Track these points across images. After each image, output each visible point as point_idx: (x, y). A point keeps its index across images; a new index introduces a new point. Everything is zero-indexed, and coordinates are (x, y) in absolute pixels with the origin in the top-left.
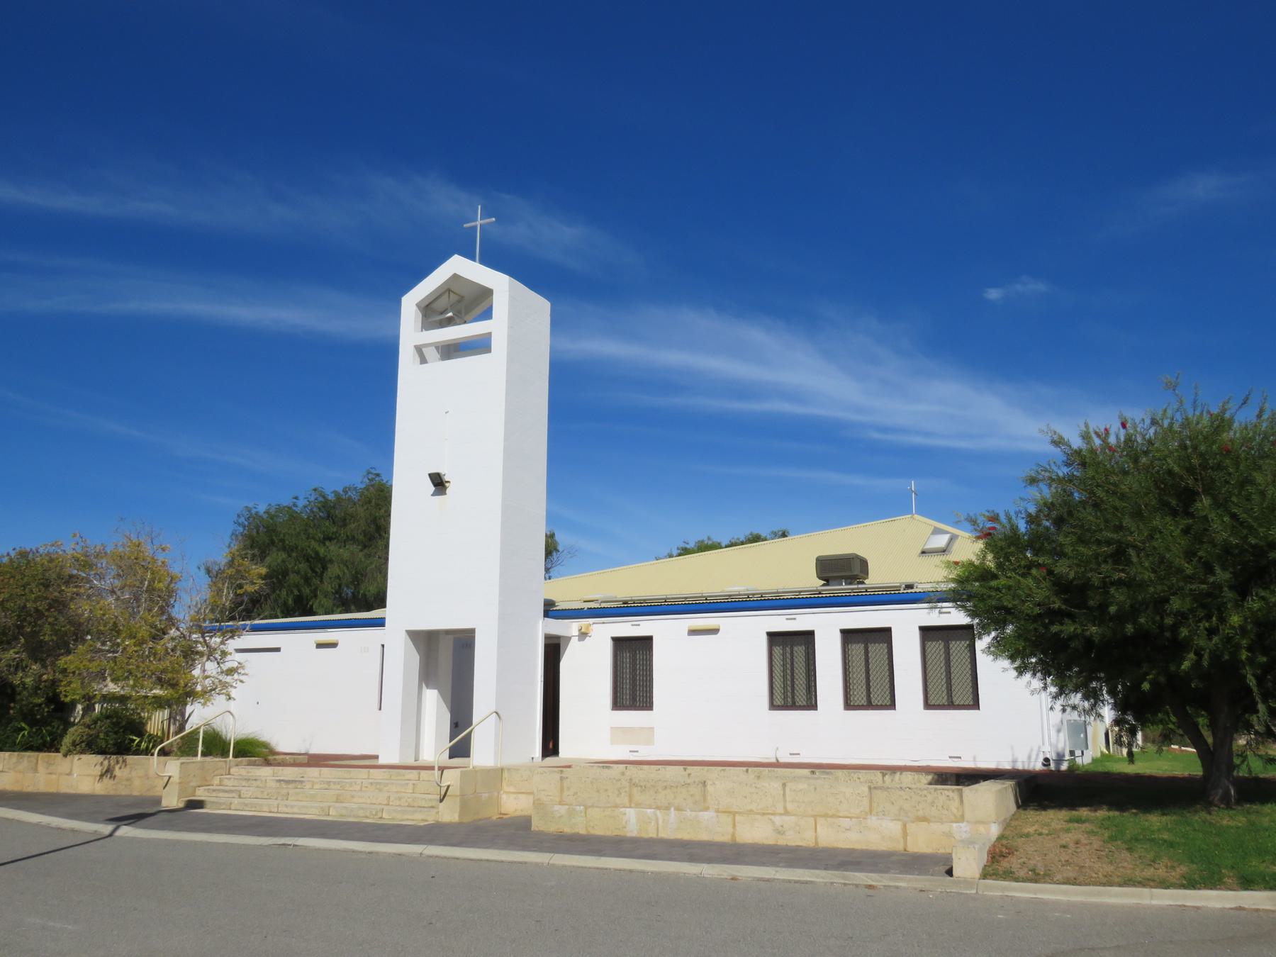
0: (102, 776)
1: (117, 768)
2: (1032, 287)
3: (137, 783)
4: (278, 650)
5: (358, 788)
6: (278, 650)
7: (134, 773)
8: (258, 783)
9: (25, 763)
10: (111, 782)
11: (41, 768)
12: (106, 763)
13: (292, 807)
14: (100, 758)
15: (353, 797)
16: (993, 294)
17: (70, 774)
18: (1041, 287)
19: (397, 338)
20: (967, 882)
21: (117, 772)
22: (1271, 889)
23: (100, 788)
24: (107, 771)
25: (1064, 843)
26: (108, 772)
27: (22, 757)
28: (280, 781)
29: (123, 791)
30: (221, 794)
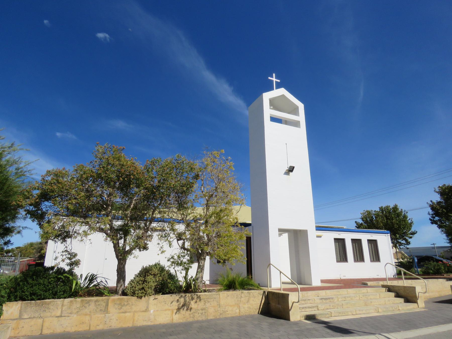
0: (179, 309)
1: (192, 302)
2: (70, 136)
3: (211, 310)
5: (358, 298)
7: (208, 305)
8: (311, 301)
9: (92, 306)
10: (188, 312)
11: (112, 308)
12: (182, 300)
13: (362, 310)
15: (371, 302)
16: (58, 134)
17: (147, 310)
18: (74, 137)
19: (317, 207)
20: (296, 323)
21: (193, 304)
23: (177, 318)
24: (183, 306)
27: (88, 302)
28: (322, 299)
29: (199, 317)
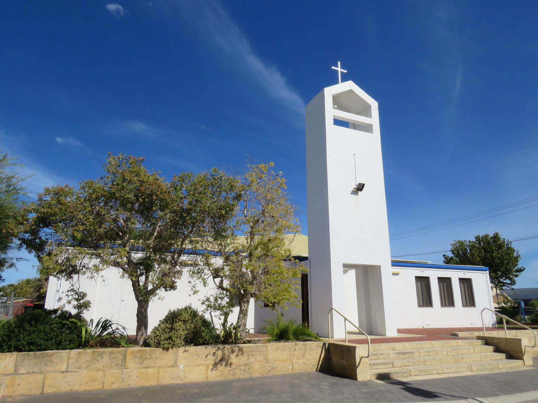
0: (216, 364)
1: (233, 356)
2: (74, 142)
3: (257, 366)
4: (29, 261)
5: (445, 353)
6: (29, 261)
7: (252, 359)
8: (384, 356)
9: (106, 359)
10: (228, 368)
11: (131, 363)
12: (220, 353)
14: (210, 349)
15: (463, 358)
16: (59, 140)
18: (79, 143)
21: (233, 359)
22: (535, 390)
23: (214, 376)
24: (221, 360)
25: (18, 383)
26: (223, 360)
28: (398, 353)
29: (241, 375)
30: (379, 367)
